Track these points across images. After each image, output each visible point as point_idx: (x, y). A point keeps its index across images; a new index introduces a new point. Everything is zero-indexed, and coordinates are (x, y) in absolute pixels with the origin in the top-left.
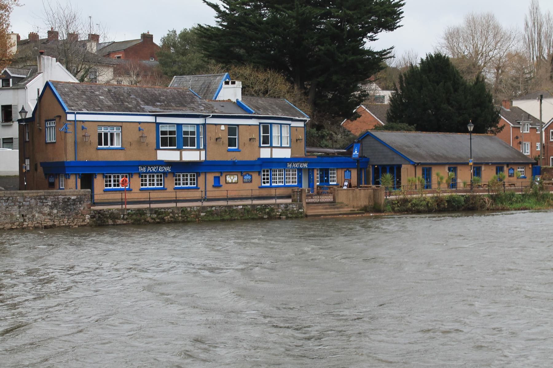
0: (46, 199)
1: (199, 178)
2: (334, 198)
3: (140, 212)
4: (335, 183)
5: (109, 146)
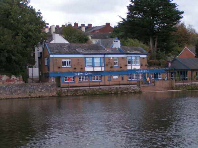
0: (39, 86)
1: (102, 77)
2: (155, 84)
3: (76, 91)
4: (161, 78)
5: (66, 66)
